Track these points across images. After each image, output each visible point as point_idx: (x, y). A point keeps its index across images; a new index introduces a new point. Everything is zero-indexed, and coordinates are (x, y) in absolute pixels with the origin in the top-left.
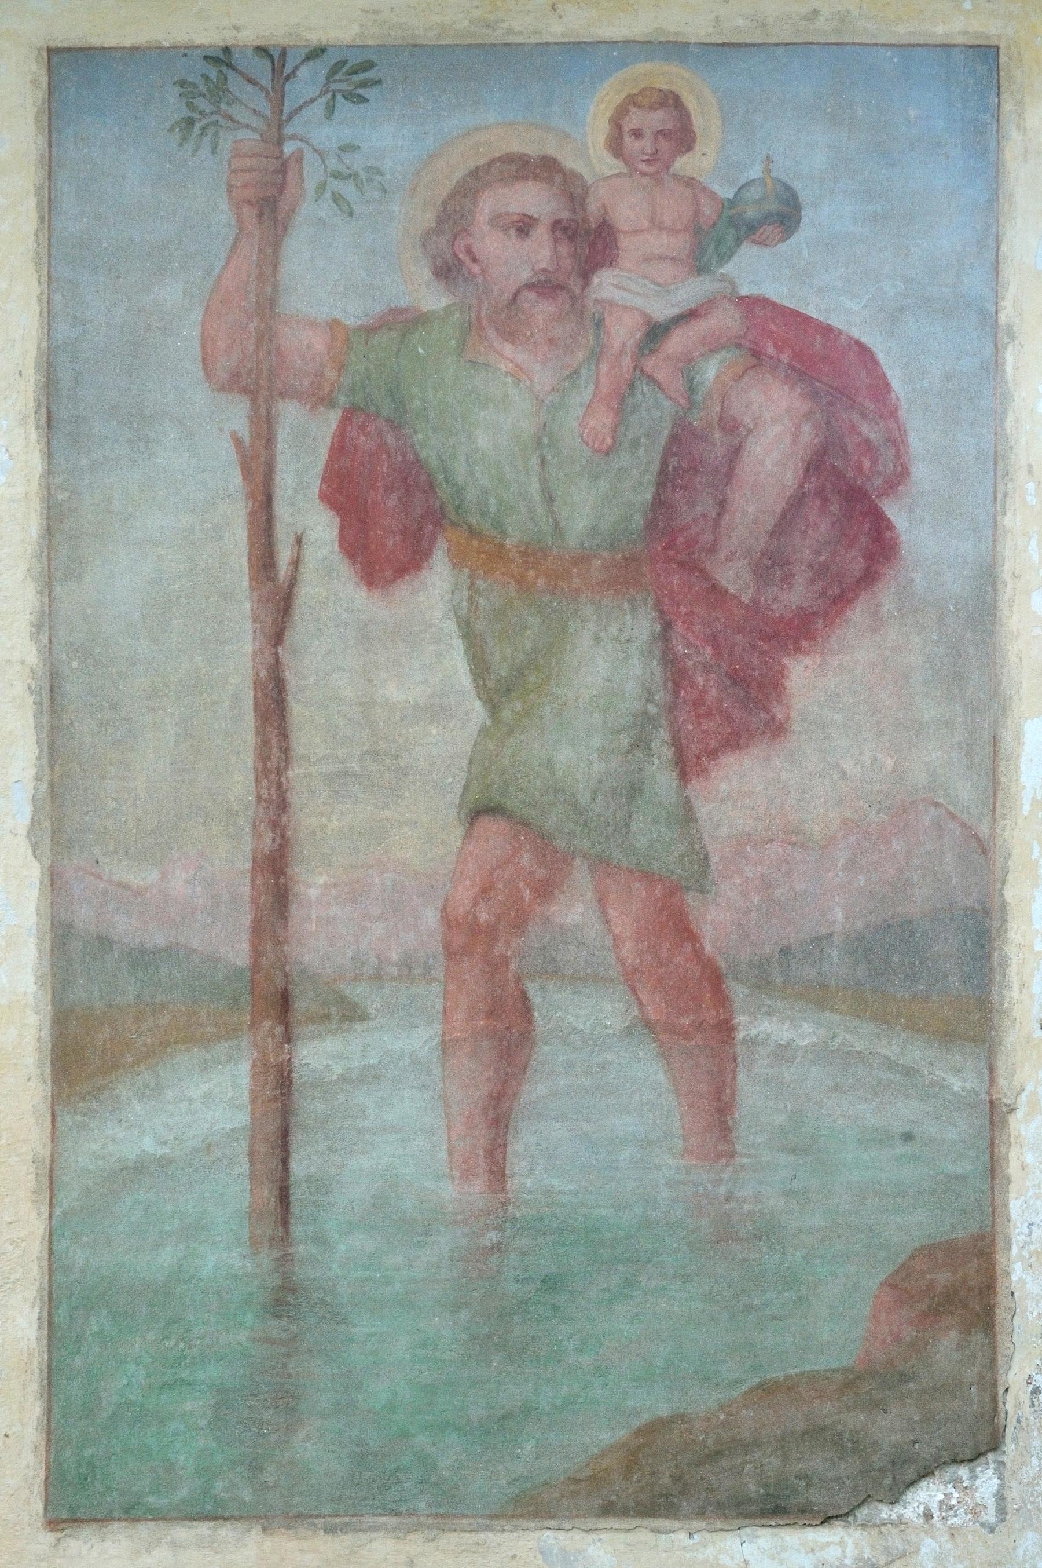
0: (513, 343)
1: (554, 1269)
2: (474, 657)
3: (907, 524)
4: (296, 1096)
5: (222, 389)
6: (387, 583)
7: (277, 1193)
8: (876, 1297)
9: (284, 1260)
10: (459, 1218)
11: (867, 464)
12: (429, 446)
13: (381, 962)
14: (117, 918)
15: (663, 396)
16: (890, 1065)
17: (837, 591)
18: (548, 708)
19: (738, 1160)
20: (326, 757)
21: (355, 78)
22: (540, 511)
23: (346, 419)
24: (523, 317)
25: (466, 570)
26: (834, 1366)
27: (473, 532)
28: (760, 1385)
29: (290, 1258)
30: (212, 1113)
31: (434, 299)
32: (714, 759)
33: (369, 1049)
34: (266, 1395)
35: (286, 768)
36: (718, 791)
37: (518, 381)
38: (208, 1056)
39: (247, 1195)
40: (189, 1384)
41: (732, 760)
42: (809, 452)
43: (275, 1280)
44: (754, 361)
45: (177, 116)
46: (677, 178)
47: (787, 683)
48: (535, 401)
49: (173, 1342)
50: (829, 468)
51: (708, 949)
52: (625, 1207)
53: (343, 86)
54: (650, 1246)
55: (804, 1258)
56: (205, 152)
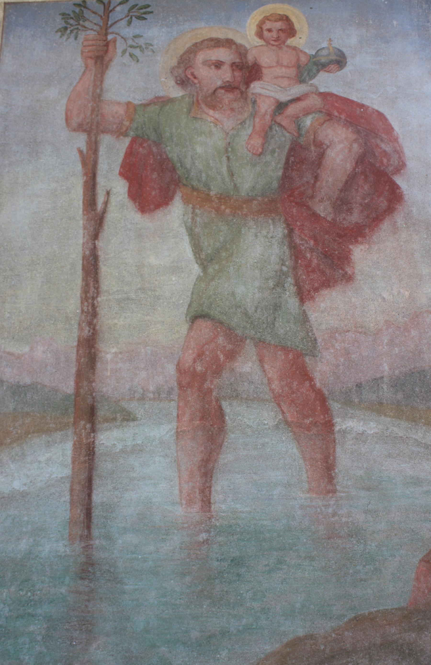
0: (214, 110)
1: (238, 554)
2: (194, 244)
3: (406, 187)
4: (96, 460)
5: (74, 130)
6: (151, 211)
7: (84, 511)
8: (418, 568)
9: (88, 547)
10: (186, 525)
11: (385, 161)
12: (173, 152)
13: (144, 391)
14: (6, 370)
15: (286, 132)
16: (418, 443)
17: (374, 216)
18: (232, 268)
19: (338, 494)
20: (117, 291)
21: (142, 11)
22: (227, 180)
23: (133, 141)
24: (218, 100)
25: (191, 206)
26: (396, 606)
27: (194, 189)
28: (355, 618)
29: (91, 547)
30: (51, 469)
31: (176, 92)
32: (317, 292)
33: (137, 435)
34: (75, 623)
35: (97, 297)
36: (319, 307)
37: (216, 125)
38: (50, 439)
39: (68, 512)
40: (33, 616)
41: (326, 292)
42: (357, 155)
43: (82, 559)
44: (328, 118)
45: (60, 27)
46: (288, 47)
47: (352, 257)
48: (224, 133)
49: (24, 592)
50: (367, 162)
51: (318, 385)
52: (277, 520)
53: (135, 14)
54: (291, 541)
55: (376, 546)
56: (72, 39)
